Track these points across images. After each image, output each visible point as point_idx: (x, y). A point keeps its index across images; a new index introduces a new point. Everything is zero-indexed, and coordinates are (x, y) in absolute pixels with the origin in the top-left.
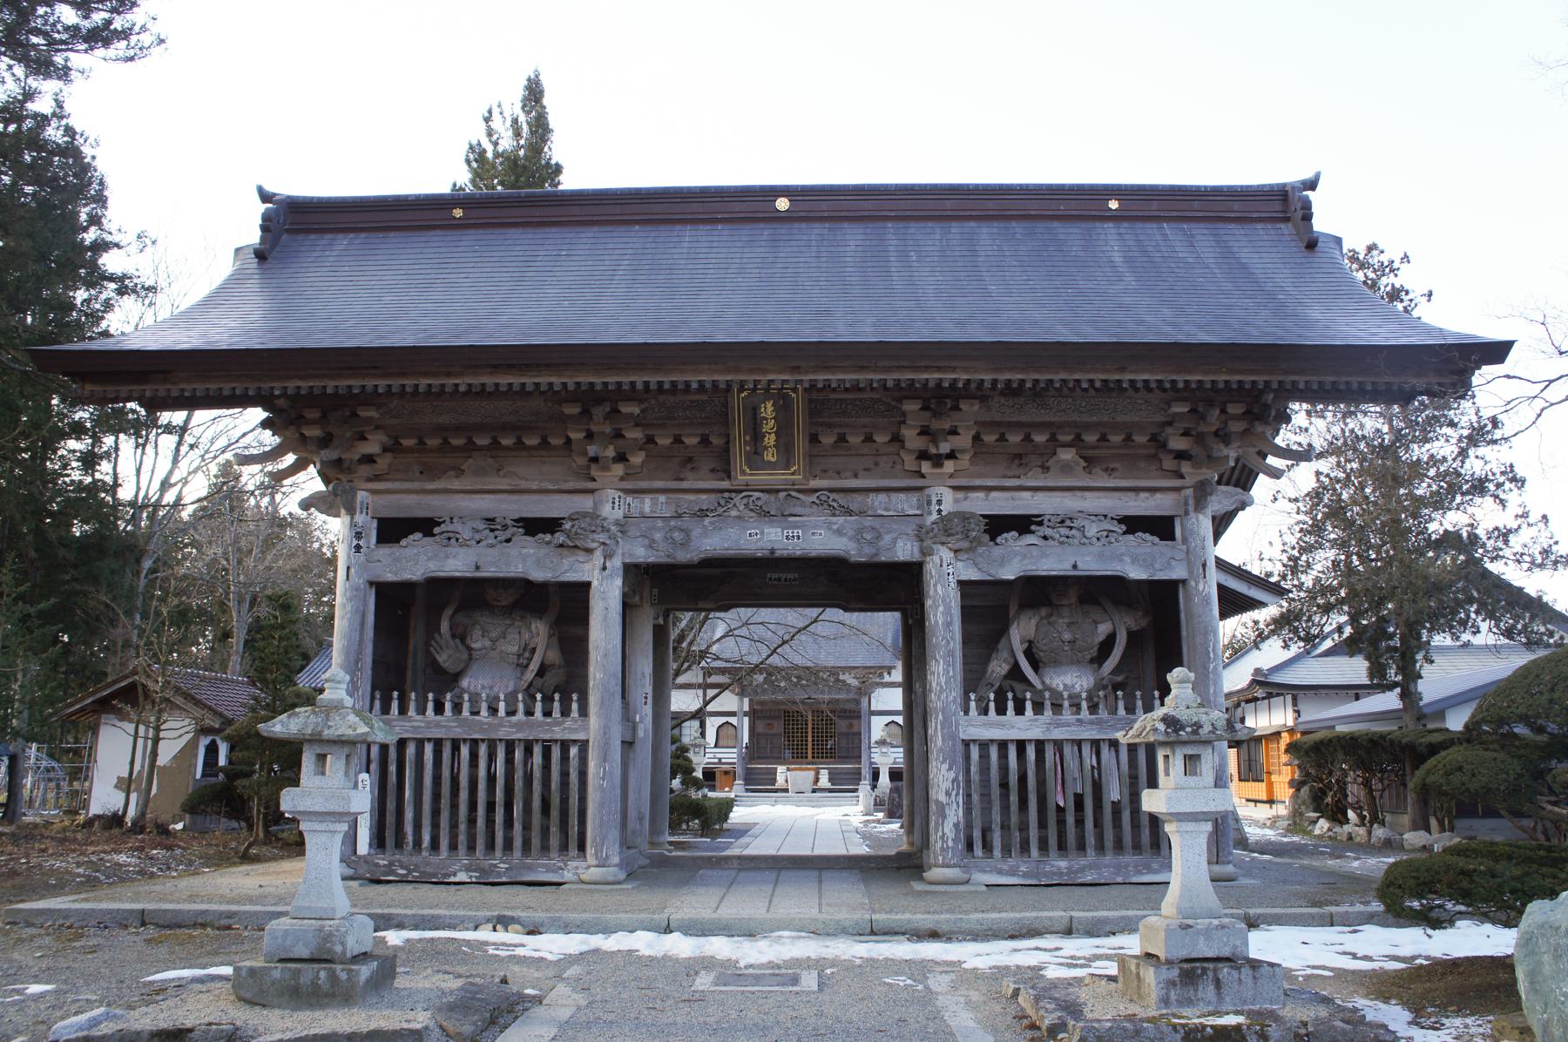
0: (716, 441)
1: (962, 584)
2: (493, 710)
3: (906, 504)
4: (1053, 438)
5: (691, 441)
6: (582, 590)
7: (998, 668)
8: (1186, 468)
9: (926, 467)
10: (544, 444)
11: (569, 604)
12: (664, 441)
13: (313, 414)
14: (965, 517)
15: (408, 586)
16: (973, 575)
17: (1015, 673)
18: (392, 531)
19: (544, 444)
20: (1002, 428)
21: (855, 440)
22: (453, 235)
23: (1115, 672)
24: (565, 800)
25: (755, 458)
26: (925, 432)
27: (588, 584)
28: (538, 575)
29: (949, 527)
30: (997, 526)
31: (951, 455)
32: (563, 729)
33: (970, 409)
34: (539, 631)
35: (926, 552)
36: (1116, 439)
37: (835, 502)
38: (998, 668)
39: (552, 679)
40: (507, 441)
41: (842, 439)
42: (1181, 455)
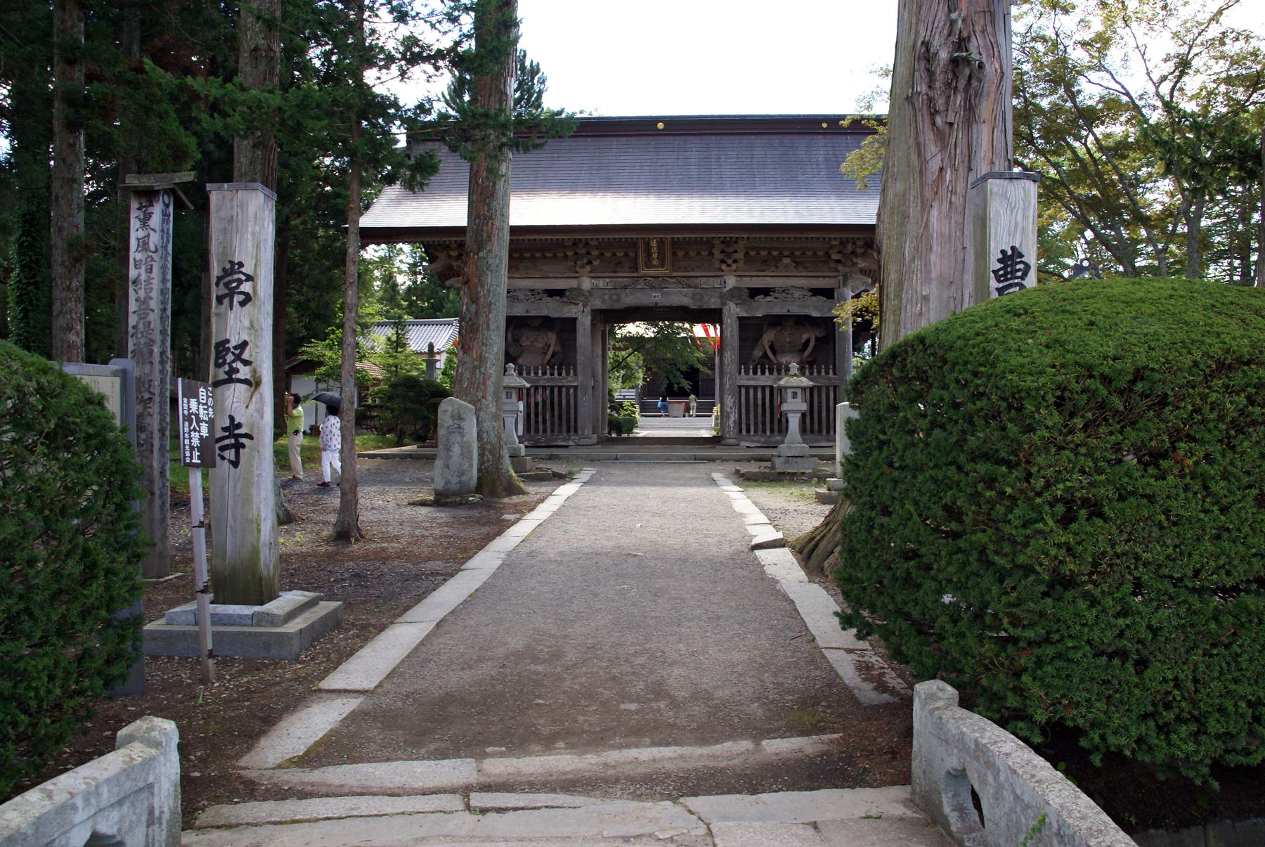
0: (632, 254)
2: (536, 373)
3: (716, 283)
4: (781, 253)
5: (620, 254)
6: (573, 321)
7: (757, 353)
8: (840, 267)
9: (724, 267)
10: (555, 256)
11: (567, 327)
12: (608, 255)
17: (765, 356)
19: (555, 256)
20: (758, 250)
21: (692, 254)
23: (810, 355)
24: (568, 413)
25: (648, 264)
26: (723, 252)
27: (575, 319)
29: (735, 293)
30: (754, 292)
32: (570, 381)
34: (552, 338)
35: (724, 304)
36: (809, 253)
37: (684, 283)
40: (538, 255)
41: (687, 253)
42: (838, 261)
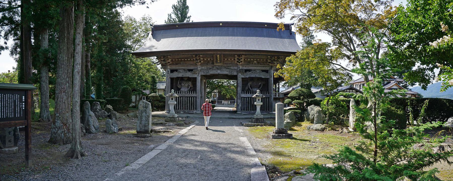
1: (242, 78)
5: (209, 59)
7: (247, 88)
13: (162, 57)
14: (242, 70)
15: (173, 78)
16: (243, 77)
18: (172, 71)
22: (177, 30)
28: (190, 77)
30: (246, 71)
31: (241, 62)
32: (194, 95)
33: (243, 56)
34: (190, 83)
35: (238, 74)
38: (247, 88)
39: (192, 89)
42: (269, 62)
